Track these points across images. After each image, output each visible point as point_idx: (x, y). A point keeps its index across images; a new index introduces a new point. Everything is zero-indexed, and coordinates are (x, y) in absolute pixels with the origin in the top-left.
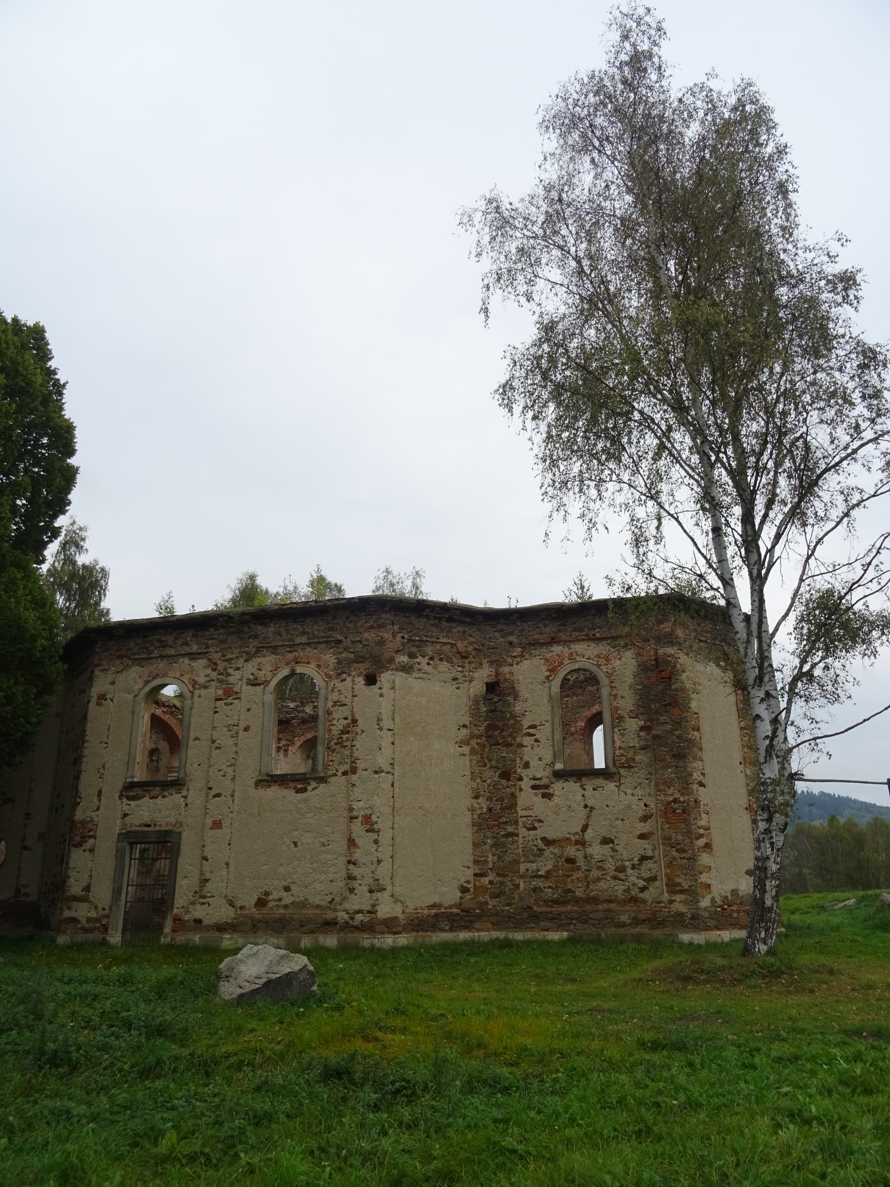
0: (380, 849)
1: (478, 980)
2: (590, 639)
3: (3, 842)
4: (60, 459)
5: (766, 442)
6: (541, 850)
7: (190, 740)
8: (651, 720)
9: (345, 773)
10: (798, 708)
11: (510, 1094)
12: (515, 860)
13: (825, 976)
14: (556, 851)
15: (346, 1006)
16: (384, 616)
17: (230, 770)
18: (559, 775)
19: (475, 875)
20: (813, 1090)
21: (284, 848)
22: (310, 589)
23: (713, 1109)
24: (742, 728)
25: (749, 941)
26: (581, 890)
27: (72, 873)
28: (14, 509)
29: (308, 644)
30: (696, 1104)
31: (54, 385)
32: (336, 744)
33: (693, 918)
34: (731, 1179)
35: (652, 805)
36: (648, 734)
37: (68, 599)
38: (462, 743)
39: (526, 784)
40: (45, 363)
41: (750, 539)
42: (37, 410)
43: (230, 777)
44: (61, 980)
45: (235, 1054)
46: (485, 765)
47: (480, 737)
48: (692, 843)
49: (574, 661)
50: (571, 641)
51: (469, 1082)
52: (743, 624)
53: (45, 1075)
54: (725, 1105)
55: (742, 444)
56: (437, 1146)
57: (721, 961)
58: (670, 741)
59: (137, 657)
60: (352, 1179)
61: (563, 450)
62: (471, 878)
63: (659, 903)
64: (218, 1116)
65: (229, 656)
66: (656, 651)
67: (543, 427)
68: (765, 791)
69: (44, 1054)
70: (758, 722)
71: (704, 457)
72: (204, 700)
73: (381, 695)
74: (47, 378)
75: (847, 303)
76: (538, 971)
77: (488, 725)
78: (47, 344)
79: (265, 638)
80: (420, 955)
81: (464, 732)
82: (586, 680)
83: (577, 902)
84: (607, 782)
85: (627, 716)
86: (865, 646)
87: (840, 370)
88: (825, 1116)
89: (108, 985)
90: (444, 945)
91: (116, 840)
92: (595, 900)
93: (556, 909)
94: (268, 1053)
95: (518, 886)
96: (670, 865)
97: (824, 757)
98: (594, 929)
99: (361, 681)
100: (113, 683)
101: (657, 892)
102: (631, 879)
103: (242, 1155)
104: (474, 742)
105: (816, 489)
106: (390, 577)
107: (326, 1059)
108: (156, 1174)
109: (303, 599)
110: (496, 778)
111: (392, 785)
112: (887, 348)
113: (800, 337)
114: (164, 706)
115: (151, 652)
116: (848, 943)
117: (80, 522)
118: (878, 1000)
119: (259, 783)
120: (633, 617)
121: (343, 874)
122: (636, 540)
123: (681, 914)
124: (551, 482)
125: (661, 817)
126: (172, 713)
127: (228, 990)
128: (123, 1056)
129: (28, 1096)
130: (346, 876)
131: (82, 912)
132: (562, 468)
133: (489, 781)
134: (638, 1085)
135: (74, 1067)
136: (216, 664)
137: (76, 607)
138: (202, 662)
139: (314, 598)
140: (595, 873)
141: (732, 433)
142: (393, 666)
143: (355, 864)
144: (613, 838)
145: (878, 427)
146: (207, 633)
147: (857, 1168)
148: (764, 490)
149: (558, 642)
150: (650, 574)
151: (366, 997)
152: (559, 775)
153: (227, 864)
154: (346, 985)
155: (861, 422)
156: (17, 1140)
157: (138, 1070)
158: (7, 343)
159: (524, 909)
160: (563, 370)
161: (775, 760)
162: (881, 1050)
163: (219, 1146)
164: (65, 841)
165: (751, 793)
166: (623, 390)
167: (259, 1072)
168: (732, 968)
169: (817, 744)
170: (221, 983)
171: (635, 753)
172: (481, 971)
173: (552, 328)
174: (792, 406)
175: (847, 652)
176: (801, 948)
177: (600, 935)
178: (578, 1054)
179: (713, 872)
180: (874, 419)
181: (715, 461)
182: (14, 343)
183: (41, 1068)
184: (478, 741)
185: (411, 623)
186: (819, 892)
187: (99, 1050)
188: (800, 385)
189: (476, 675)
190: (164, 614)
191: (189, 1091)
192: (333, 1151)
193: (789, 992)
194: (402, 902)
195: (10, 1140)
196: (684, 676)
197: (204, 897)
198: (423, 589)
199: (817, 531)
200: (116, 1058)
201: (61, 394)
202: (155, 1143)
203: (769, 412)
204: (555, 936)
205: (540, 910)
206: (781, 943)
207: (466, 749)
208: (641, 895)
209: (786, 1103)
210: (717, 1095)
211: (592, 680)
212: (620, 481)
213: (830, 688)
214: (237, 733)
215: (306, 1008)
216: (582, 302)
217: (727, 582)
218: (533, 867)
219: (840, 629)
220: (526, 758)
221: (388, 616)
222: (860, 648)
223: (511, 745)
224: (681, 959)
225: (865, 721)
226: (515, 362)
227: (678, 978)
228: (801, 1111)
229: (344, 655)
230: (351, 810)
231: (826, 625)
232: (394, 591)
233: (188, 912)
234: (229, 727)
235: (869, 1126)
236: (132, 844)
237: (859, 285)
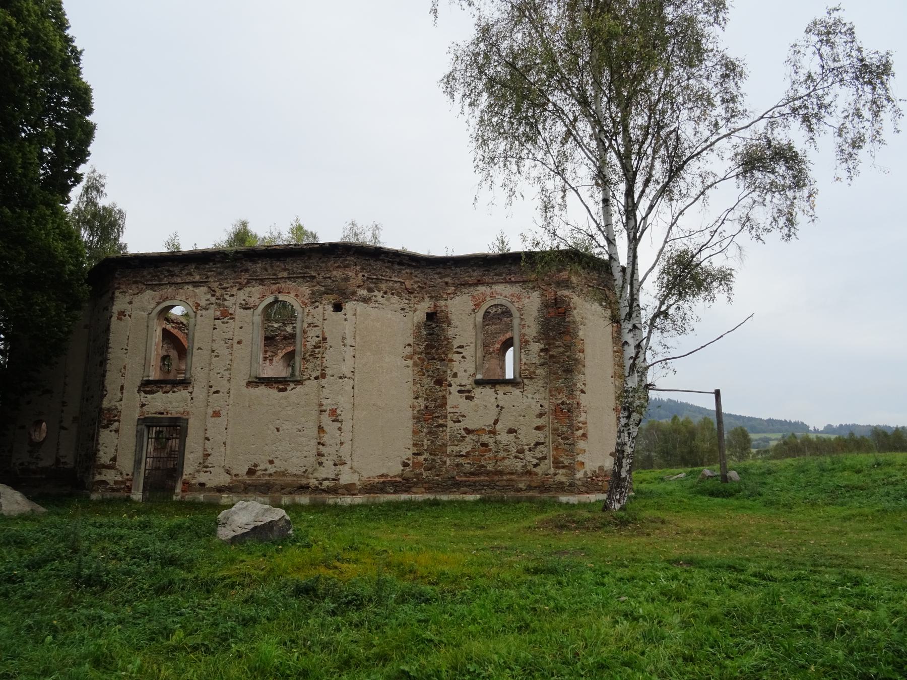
0: (343, 434)
1: (413, 528)
2: (507, 282)
3: (44, 423)
4: (79, 116)
5: (648, 134)
6: (463, 437)
7: (194, 350)
8: (549, 344)
9: (317, 378)
10: (656, 336)
11: (431, 604)
12: (443, 444)
13: (659, 525)
14: (474, 438)
15: (314, 544)
16: (349, 258)
17: (226, 373)
18: (478, 383)
19: (414, 454)
20: (642, 599)
21: (269, 432)
22: (291, 235)
23: (572, 612)
25: (608, 501)
27: (101, 448)
28: (42, 157)
29: (289, 278)
30: (561, 609)
31: (72, 51)
32: (310, 356)
33: (570, 485)
34: (581, 656)
35: (546, 406)
37: (91, 234)
38: (407, 358)
39: (454, 389)
40: (63, 31)
41: (630, 209)
42: (58, 73)
44: (94, 525)
45: (229, 578)
47: (421, 353)
48: (573, 433)
49: (494, 298)
50: (492, 283)
51: (402, 596)
52: (621, 274)
53: (82, 592)
54: (581, 609)
55: (629, 135)
56: (377, 638)
57: (587, 515)
58: (562, 360)
59: (150, 283)
60: (314, 660)
61: (492, 131)
62: (411, 456)
63: (547, 475)
64: (215, 620)
66: (556, 294)
67: (477, 113)
68: (627, 397)
69: (81, 577)
70: (626, 347)
71: (600, 142)
72: (205, 319)
73: (346, 320)
74: (65, 44)
75: (717, 23)
76: (457, 521)
77: (427, 345)
78: (64, 14)
79: (254, 272)
80: (371, 510)
81: (409, 349)
82: (503, 313)
83: (488, 474)
84: (514, 389)
85: (531, 341)
86: (707, 293)
87: (708, 78)
88: (648, 615)
89: (131, 529)
90: (389, 503)
91: (136, 424)
92: (501, 473)
93: (472, 479)
94: (254, 577)
95: (445, 463)
96: (556, 448)
97: (671, 373)
98: (499, 493)
99: (330, 308)
100: (131, 303)
101: (547, 467)
103: (233, 645)
104: (416, 357)
105: (682, 172)
106: (355, 228)
107: (297, 581)
108: (168, 659)
109: (286, 243)
110: (432, 385)
111: (353, 388)
112: (743, 62)
113: (680, 49)
114: (173, 322)
115: (161, 280)
116: (677, 503)
117: (100, 171)
118: (693, 540)
119: (249, 384)
120: (539, 266)
121: (315, 452)
122: (545, 206)
123: (562, 483)
124: (482, 158)
125: (552, 414)
126: (180, 329)
127: (225, 533)
128: (143, 579)
129: (69, 607)
131: (110, 476)
132: (491, 146)
133: (426, 386)
134: (522, 596)
135: (105, 587)
136: (214, 291)
137: (98, 241)
138: (204, 289)
139: (293, 242)
140: (502, 454)
141: (623, 125)
142: (355, 298)
143: (323, 445)
145: (730, 125)
146: (207, 266)
147: (666, 647)
148: (643, 172)
149: (483, 284)
150: (554, 233)
151: (329, 539)
152: (478, 383)
153: (224, 443)
154: (315, 530)
155: (719, 121)
156: (61, 637)
157: (154, 589)
158: (28, 11)
160: (496, 66)
161: (636, 375)
162: (691, 572)
163: (216, 639)
164: (95, 423)
165: (618, 398)
166: (541, 85)
167: (247, 590)
168: (594, 519)
169: (667, 364)
170: (219, 528)
171: (536, 368)
172: (416, 521)
173: (488, 30)
174: (669, 106)
175: (694, 296)
176: (644, 506)
177: (503, 497)
178: (481, 577)
179: (587, 454)
180: (729, 119)
181: (608, 147)
182: (35, 12)
183: (78, 587)
184: (419, 356)
185: (370, 265)
186: (660, 468)
187: (124, 574)
188: (677, 89)
189: (419, 306)
190: (171, 250)
191: (194, 602)
192: (300, 642)
193: (633, 535)
195: (54, 637)
196: (575, 312)
197: (207, 467)
198: (381, 239)
199: (678, 205)
200: (137, 580)
201: (78, 59)
202: (168, 638)
203: (652, 109)
204: (471, 497)
205: (460, 479)
206: (631, 502)
209: (624, 607)
210: (576, 603)
211: (507, 313)
212: (535, 159)
213: (679, 323)
215: (283, 546)
216: (513, 9)
217: (611, 242)
218: (457, 449)
219: (690, 279)
221: (352, 258)
222: (703, 294)
223: (444, 360)
224: (560, 513)
225: (702, 347)
226: (457, 57)
227: (556, 527)
228: (632, 612)
229: (317, 288)
230: (321, 405)
231: (680, 276)
232: (358, 239)
233: (194, 478)
234: (226, 341)
235: (677, 621)
236: (149, 427)
237: (727, 9)
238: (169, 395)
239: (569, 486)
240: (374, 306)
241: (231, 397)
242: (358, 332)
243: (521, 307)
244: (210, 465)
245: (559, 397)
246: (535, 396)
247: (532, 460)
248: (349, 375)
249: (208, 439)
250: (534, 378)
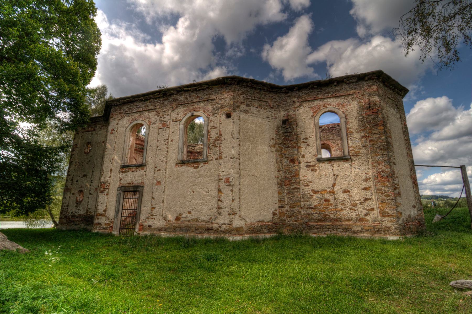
0: (234, 194)
6: (311, 196)
7: (148, 147)
9: (216, 159)
14: (319, 196)
17: (165, 159)
19: (279, 207)
26: (333, 215)
32: (212, 146)
36: (366, 139)
38: (272, 146)
39: (302, 165)
46: (283, 157)
47: (280, 144)
58: (378, 142)
62: (278, 209)
65: (165, 110)
81: (272, 141)
91: (117, 190)
93: (319, 223)
95: (300, 212)
96: (382, 202)
99: (224, 116)
100: (117, 124)
102: (359, 209)
104: (277, 146)
110: (288, 163)
111: (239, 164)
119: (177, 164)
121: (216, 206)
130: (217, 207)
133: (284, 164)
136: (159, 113)
138: (154, 113)
140: (340, 207)
143: (221, 201)
144: (349, 189)
153: (163, 201)
159: (304, 223)
194: (244, 220)
197: (152, 215)
205: (312, 224)
207: (274, 149)
208: (366, 217)
214: (168, 143)
230: (219, 176)
238: (134, 173)
239: (394, 229)
240: (250, 114)
243: (344, 111)
245: (381, 166)
247: (363, 211)
248: (236, 156)
249: (153, 198)
250: (358, 156)
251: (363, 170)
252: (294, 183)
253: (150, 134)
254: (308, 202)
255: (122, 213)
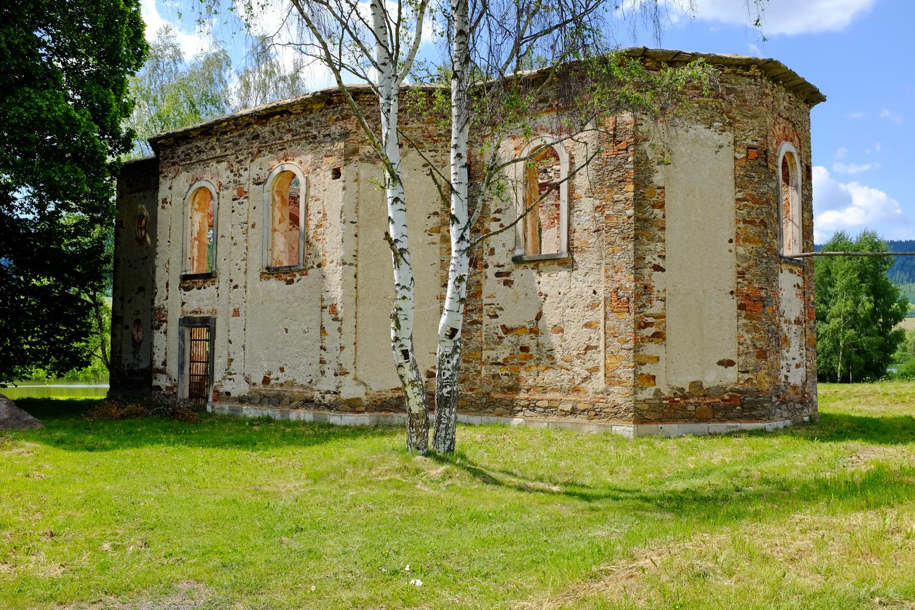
6: (500, 338)
7: (219, 238)
14: (513, 339)
24: (738, 200)
29: (293, 141)
39: (491, 271)
43: (243, 270)
65: (241, 158)
81: (435, 220)
85: (583, 195)
95: (479, 372)
100: (170, 188)
102: (576, 369)
111: (355, 276)
143: (325, 350)
153: (244, 347)
159: (483, 394)
179: (662, 363)
194: (365, 385)
197: (230, 374)
218: (493, 354)
220: (492, 245)
230: (322, 300)
238: (201, 291)
241: (248, 293)
242: (361, 203)
244: (233, 372)
246: (586, 279)
249: (230, 342)
251: (589, 284)
252: (473, 310)
253: (220, 210)
254: (494, 352)
255: (190, 369)
